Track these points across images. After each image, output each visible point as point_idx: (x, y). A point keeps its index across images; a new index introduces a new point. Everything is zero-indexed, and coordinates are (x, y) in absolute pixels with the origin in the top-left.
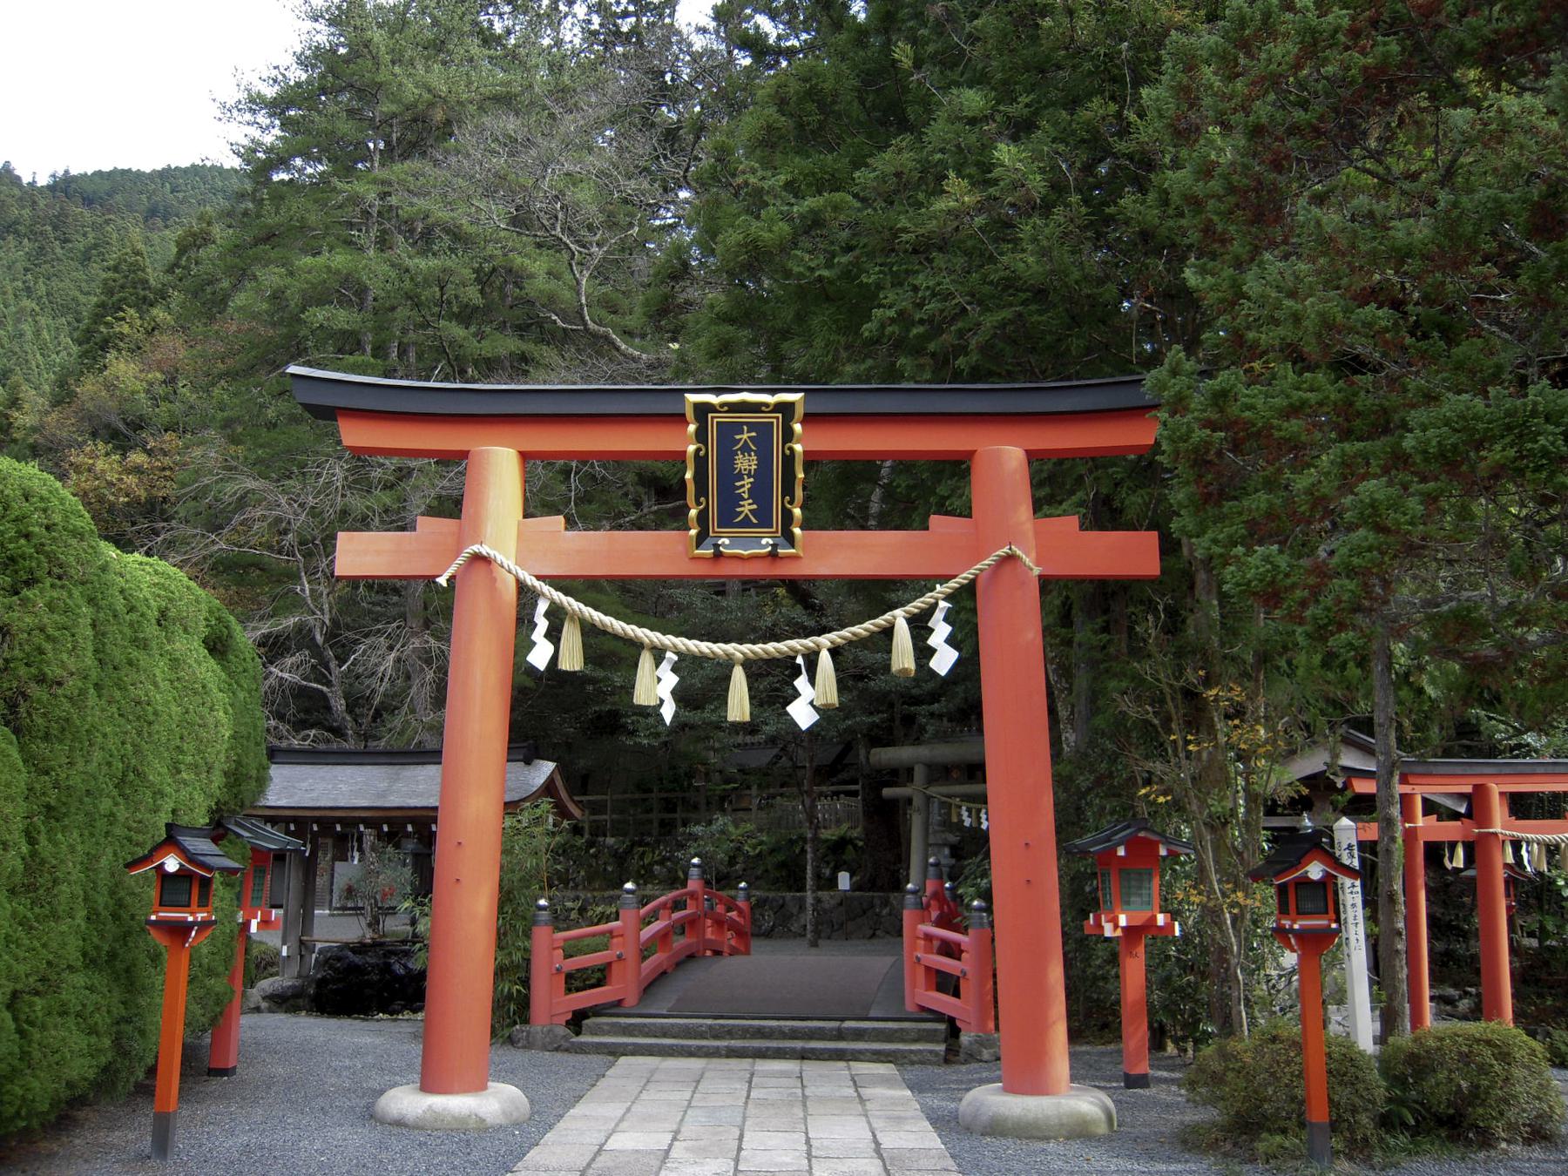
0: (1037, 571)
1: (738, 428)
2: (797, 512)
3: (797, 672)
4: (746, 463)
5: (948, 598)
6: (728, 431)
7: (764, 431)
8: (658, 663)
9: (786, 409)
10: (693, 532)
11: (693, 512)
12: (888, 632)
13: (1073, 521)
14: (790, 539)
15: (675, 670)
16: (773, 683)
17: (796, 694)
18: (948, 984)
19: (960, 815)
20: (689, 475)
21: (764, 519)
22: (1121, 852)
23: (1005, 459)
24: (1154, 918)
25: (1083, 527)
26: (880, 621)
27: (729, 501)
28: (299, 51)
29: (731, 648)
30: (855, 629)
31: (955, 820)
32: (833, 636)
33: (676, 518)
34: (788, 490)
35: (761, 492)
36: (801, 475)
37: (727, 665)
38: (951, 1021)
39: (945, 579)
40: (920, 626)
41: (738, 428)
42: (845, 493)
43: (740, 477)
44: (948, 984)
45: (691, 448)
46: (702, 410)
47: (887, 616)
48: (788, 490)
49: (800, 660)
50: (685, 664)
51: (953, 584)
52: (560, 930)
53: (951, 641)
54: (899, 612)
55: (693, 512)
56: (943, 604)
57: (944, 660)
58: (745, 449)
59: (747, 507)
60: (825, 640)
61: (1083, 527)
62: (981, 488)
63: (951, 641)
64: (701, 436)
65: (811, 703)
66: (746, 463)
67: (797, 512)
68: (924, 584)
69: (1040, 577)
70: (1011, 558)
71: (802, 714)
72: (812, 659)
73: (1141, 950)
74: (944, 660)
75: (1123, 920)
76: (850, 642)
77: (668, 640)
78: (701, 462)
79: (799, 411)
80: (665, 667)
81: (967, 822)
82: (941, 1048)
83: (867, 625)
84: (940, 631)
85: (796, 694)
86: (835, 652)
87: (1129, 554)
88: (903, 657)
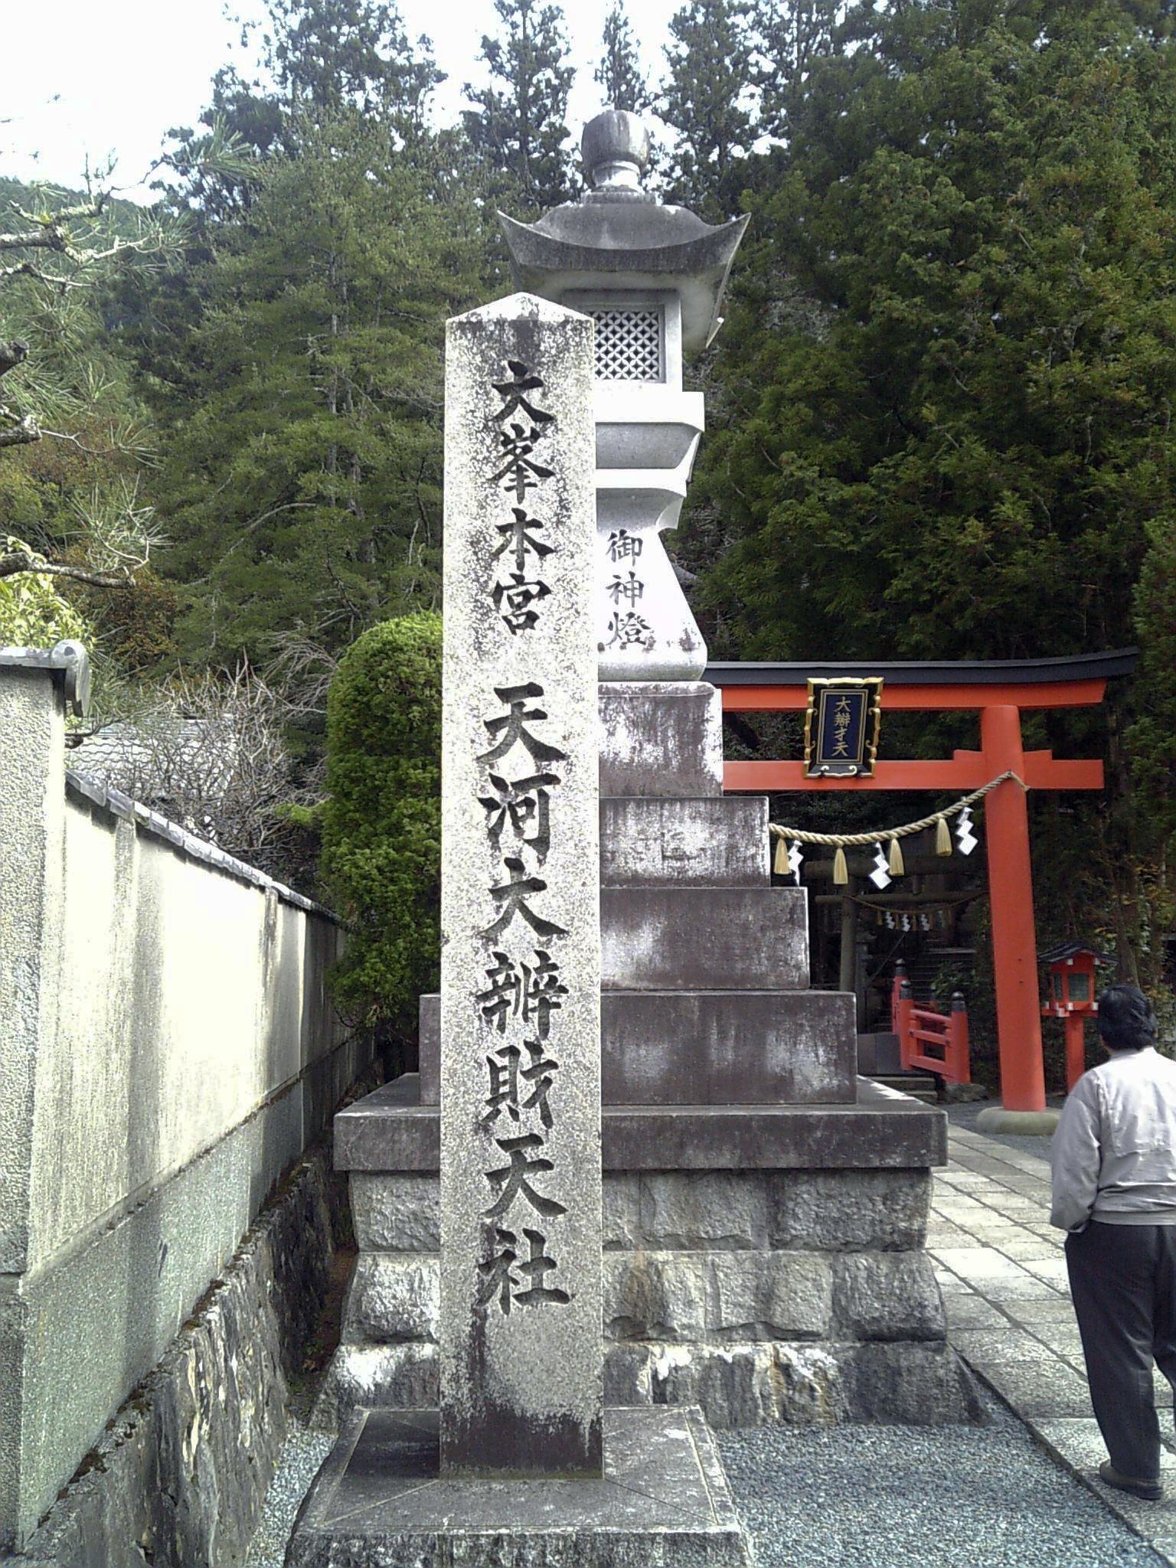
0: (1027, 788)
1: (839, 698)
2: (874, 749)
3: (876, 853)
4: (842, 720)
5: (970, 806)
6: (832, 700)
7: (855, 701)
8: (789, 848)
9: (872, 688)
10: (807, 762)
11: (808, 750)
12: (934, 826)
13: (1048, 752)
14: (867, 766)
15: (800, 850)
16: (862, 857)
17: (875, 867)
18: (932, 1050)
19: (884, 920)
20: (807, 728)
21: (851, 754)
22: (1070, 962)
23: (1003, 713)
24: (1089, 1005)
25: (1055, 757)
26: (928, 820)
27: (830, 742)
28: (471, 382)
29: (835, 837)
30: (913, 825)
31: (880, 923)
32: (898, 829)
33: (798, 755)
34: (869, 735)
35: (851, 738)
36: (878, 728)
37: (833, 847)
38: (936, 1075)
39: (968, 793)
40: (953, 823)
41: (839, 698)
42: (906, 735)
43: (838, 728)
44: (932, 1050)
45: (810, 711)
46: (818, 688)
47: (932, 817)
48: (869, 735)
49: (878, 845)
50: (807, 849)
51: (973, 796)
52: (916, 1007)
53: (972, 832)
54: (939, 815)
55: (808, 750)
56: (967, 810)
57: (968, 845)
58: (843, 711)
59: (841, 747)
60: (894, 833)
61: (1055, 757)
62: (989, 732)
63: (972, 832)
64: (816, 704)
65: (887, 872)
66: (842, 720)
67: (874, 749)
68: (950, 797)
69: (1027, 793)
70: (1009, 779)
71: (880, 878)
72: (886, 844)
73: (1081, 1026)
74: (968, 845)
75: (1070, 1007)
76: (910, 834)
77: (795, 832)
78: (815, 719)
79: (880, 688)
80: (794, 850)
81: (891, 925)
82: (934, 1093)
83: (920, 823)
84: (965, 827)
85: (875, 867)
86: (900, 839)
87: (1083, 774)
88: (944, 845)
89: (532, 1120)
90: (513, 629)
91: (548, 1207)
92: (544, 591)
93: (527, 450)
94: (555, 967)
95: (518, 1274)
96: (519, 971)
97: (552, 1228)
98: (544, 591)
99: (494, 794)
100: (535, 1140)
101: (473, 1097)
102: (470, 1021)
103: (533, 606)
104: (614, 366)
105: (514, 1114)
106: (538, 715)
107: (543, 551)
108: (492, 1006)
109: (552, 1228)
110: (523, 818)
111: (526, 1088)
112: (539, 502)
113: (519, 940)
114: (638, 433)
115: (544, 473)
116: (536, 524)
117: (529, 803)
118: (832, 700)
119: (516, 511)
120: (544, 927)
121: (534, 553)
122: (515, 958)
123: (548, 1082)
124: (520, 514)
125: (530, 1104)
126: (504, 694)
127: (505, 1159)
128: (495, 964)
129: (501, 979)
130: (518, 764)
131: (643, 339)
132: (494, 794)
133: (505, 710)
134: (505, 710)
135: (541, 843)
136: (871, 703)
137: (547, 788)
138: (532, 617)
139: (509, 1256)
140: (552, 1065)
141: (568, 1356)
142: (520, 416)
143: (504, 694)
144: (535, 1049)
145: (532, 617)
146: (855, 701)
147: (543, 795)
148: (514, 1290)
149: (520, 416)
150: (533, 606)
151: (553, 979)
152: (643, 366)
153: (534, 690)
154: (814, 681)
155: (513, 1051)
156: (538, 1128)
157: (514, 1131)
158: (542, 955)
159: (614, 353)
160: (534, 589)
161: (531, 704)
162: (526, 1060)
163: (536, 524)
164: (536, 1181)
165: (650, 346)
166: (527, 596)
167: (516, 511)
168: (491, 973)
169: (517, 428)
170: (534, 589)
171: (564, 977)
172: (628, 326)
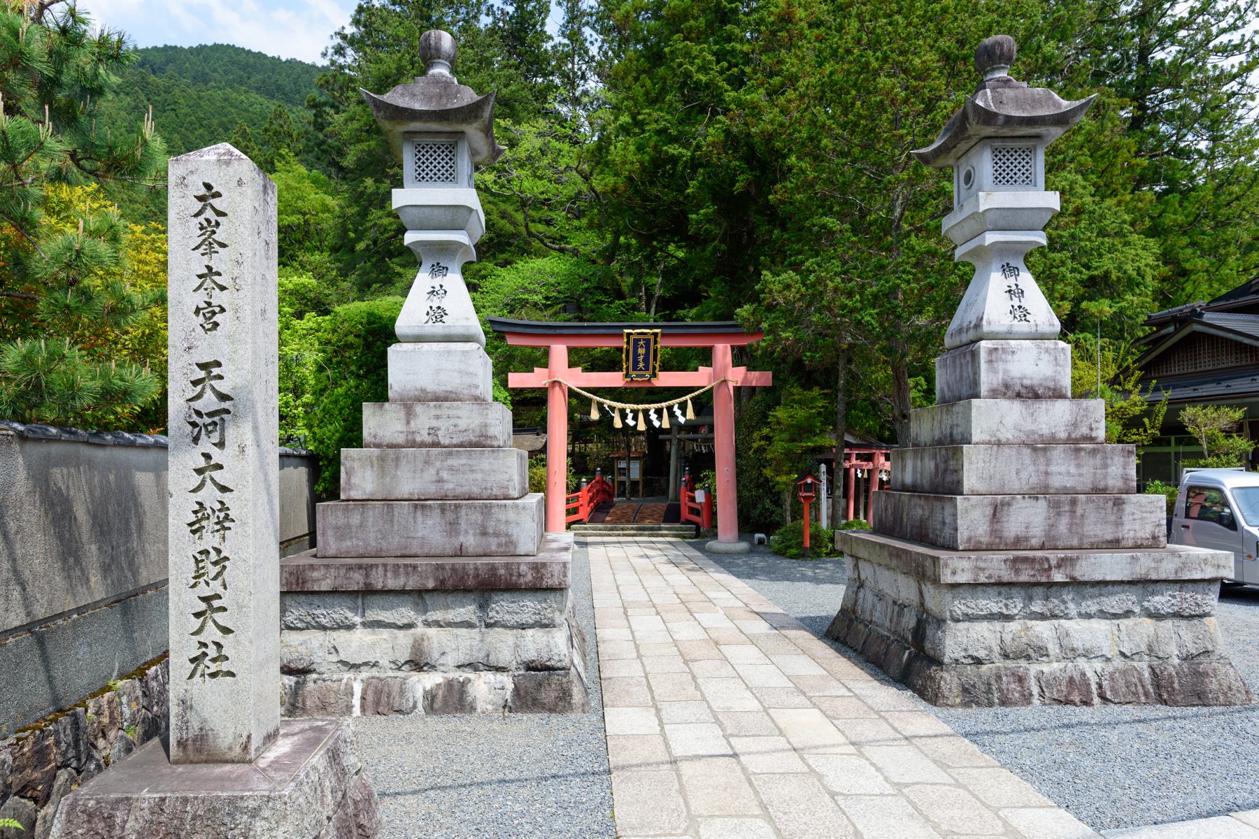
4: (641, 351)
6: (636, 341)
7: (647, 342)
9: (656, 335)
21: (647, 368)
34: (655, 359)
35: (646, 360)
38: (697, 524)
46: (629, 335)
48: (655, 359)
59: (641, 365)
64: (628, 343)
66: (641, 351)
89: (216, 587)
90: (207, 330)
91: (226, 631)
92: (223, 310)
93: (214, 232)
94: (228, 509)
95: (209, 664)
96: (209, 511)
97: (226, 641)
98: (223, 310)
99: (195, 418)
100: (218, 597)
101: (184, 576)
102: (183, 536)
103: (217, 318)
104: (431, 174)
105: (207, 584)
106: (220, 377)
107: (223, 288)
108: (196, 529)
109: (226, 641)
110: (211, 432)
111: (213, 570)
112: (220, 261)
113: (210, 496)
114: (442, 211)
115: (223, 245)
116: (219, 274)
117: (215, 424)
118: (636, 341)
119: (207, 267)
120: (224, 489)
121: (217, 290)
122: (207, 505)
123: (224, 567)
124: (209, 268)
125: (215, 578)
126: (202, 366)
127: (203, 606)
128: (197, 507)
129: (200, 515)
130: (209, 402)
131: (447, 159)
132: (195, 418)
133: (202, 374)
134: (202, 374)
135: (221, 445)
136: (656, 342)
137: (225, 416)
138: (216, 325)
139: (205, 655)
140: (226, 559)
141: (235, 704)
142: (209, 213)
143: (202, 366)
144: (218, 551)
145: (216, 325)
146: (647, 342)
147: (222, 419)
148: (207, 671)
149: (209, 213)
150: (217, 318)
151: (227, 515)
152: (447, 174)
153: (218, 364)
154: (627, 331)
155: (205, 552)
156: (220, 590)
157: (207, 592)
158: (222, 503)
159: (431, 167)
160: (217, 310)
161: (215, 371)
162: (214, 556)
163: (219, 274)
164: (219, 617)
165: (451, 163)
166: (214, 313)
167: (207, 267)
168: (195, 512)
169: (208, 221)
170: (217, 310)
171: (232, 514)
172: (439, 152)
